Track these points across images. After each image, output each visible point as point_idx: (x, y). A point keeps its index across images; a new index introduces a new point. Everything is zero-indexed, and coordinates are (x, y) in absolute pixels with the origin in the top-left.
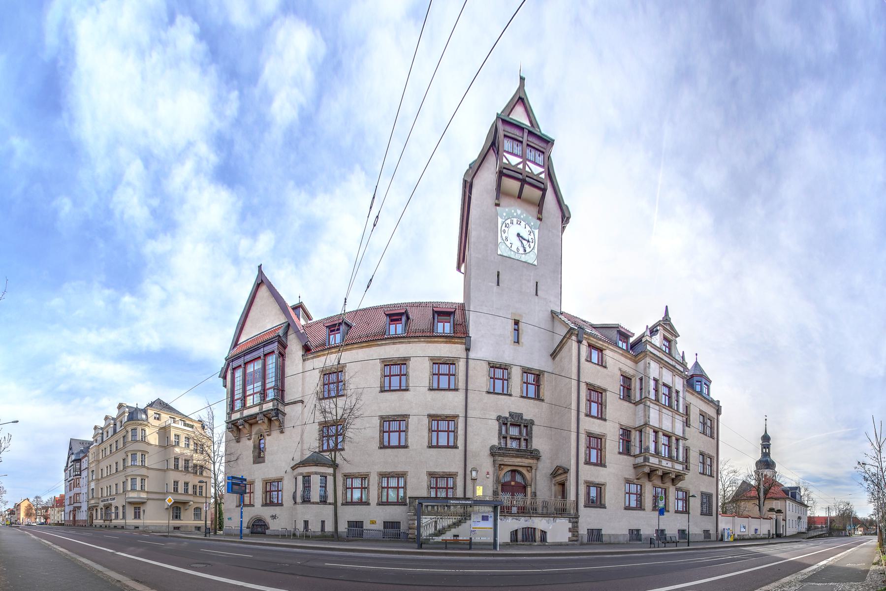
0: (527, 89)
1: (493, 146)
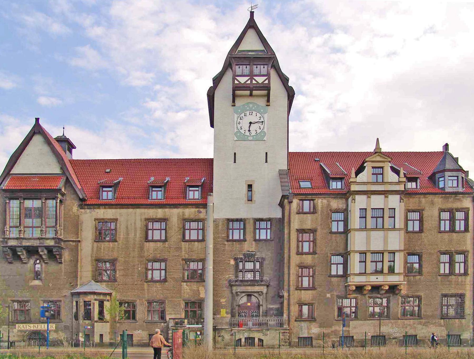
0: (255, 18)
1: (228, 65)
